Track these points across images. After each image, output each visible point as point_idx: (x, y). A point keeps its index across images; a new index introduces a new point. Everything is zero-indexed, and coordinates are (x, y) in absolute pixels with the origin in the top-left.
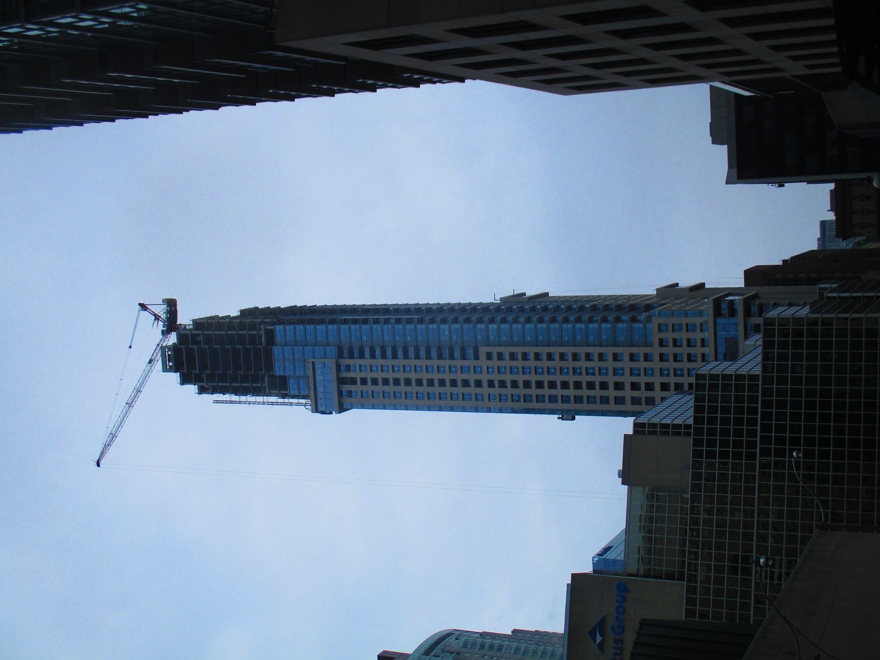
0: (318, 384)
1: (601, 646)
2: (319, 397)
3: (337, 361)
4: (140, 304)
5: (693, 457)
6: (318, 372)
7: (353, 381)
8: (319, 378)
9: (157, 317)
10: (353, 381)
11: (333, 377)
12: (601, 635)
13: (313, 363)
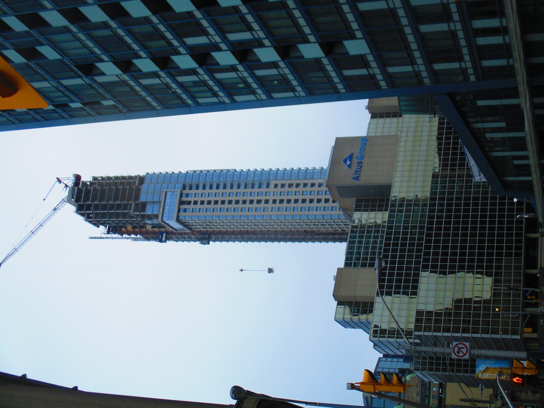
0: (166, 204)
1: (349, 166)
2: (165, 212)
3: (181, 191)
4: (57, 178)
5: (379, 282)
6: (168, 197)
7: (189, 203)
8: (168, 201)
9: (66, 186)
10: (189, 203)
11: (177, 201)
12: (350, 161)
13: (166, 192)
